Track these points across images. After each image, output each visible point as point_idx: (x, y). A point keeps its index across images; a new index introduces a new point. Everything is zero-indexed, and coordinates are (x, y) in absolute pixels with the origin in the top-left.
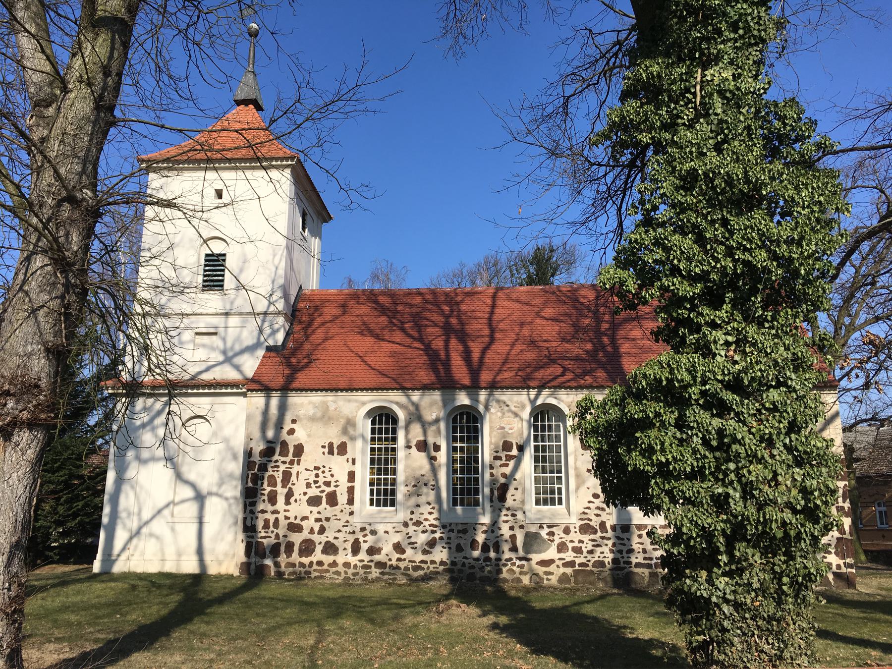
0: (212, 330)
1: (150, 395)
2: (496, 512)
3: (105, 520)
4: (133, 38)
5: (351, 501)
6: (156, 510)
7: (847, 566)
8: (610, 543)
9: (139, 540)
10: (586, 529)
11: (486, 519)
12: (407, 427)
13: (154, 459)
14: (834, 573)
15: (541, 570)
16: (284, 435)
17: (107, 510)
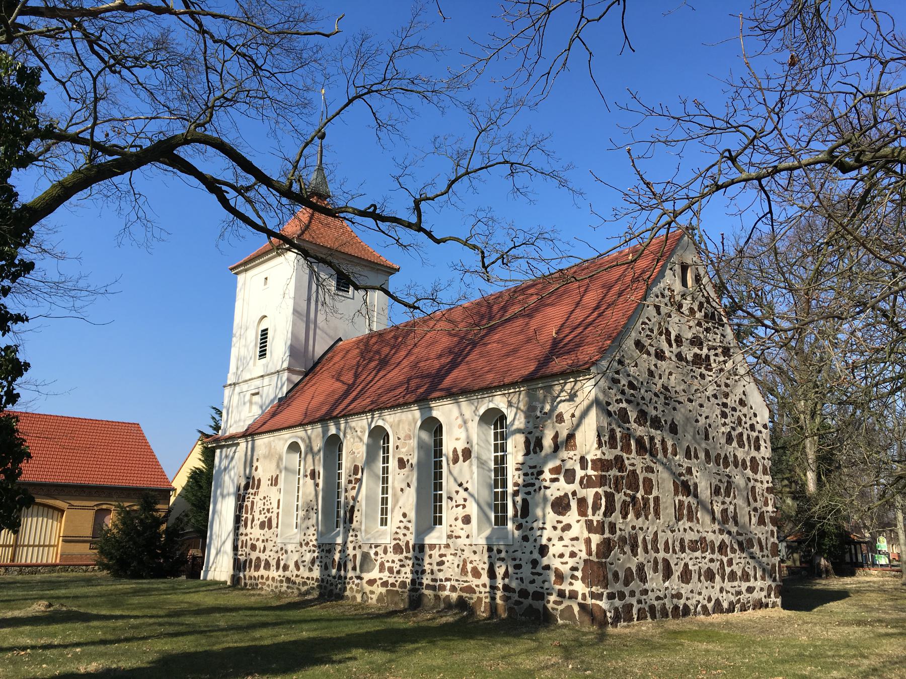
1: (228, 446)
2: (347, 531)
5: (277, 527)
7: (593, 596)
8: (410, 563)
10: (397, 549)
11: (339, 540)
14: (580, 604)
15: (368, 588)
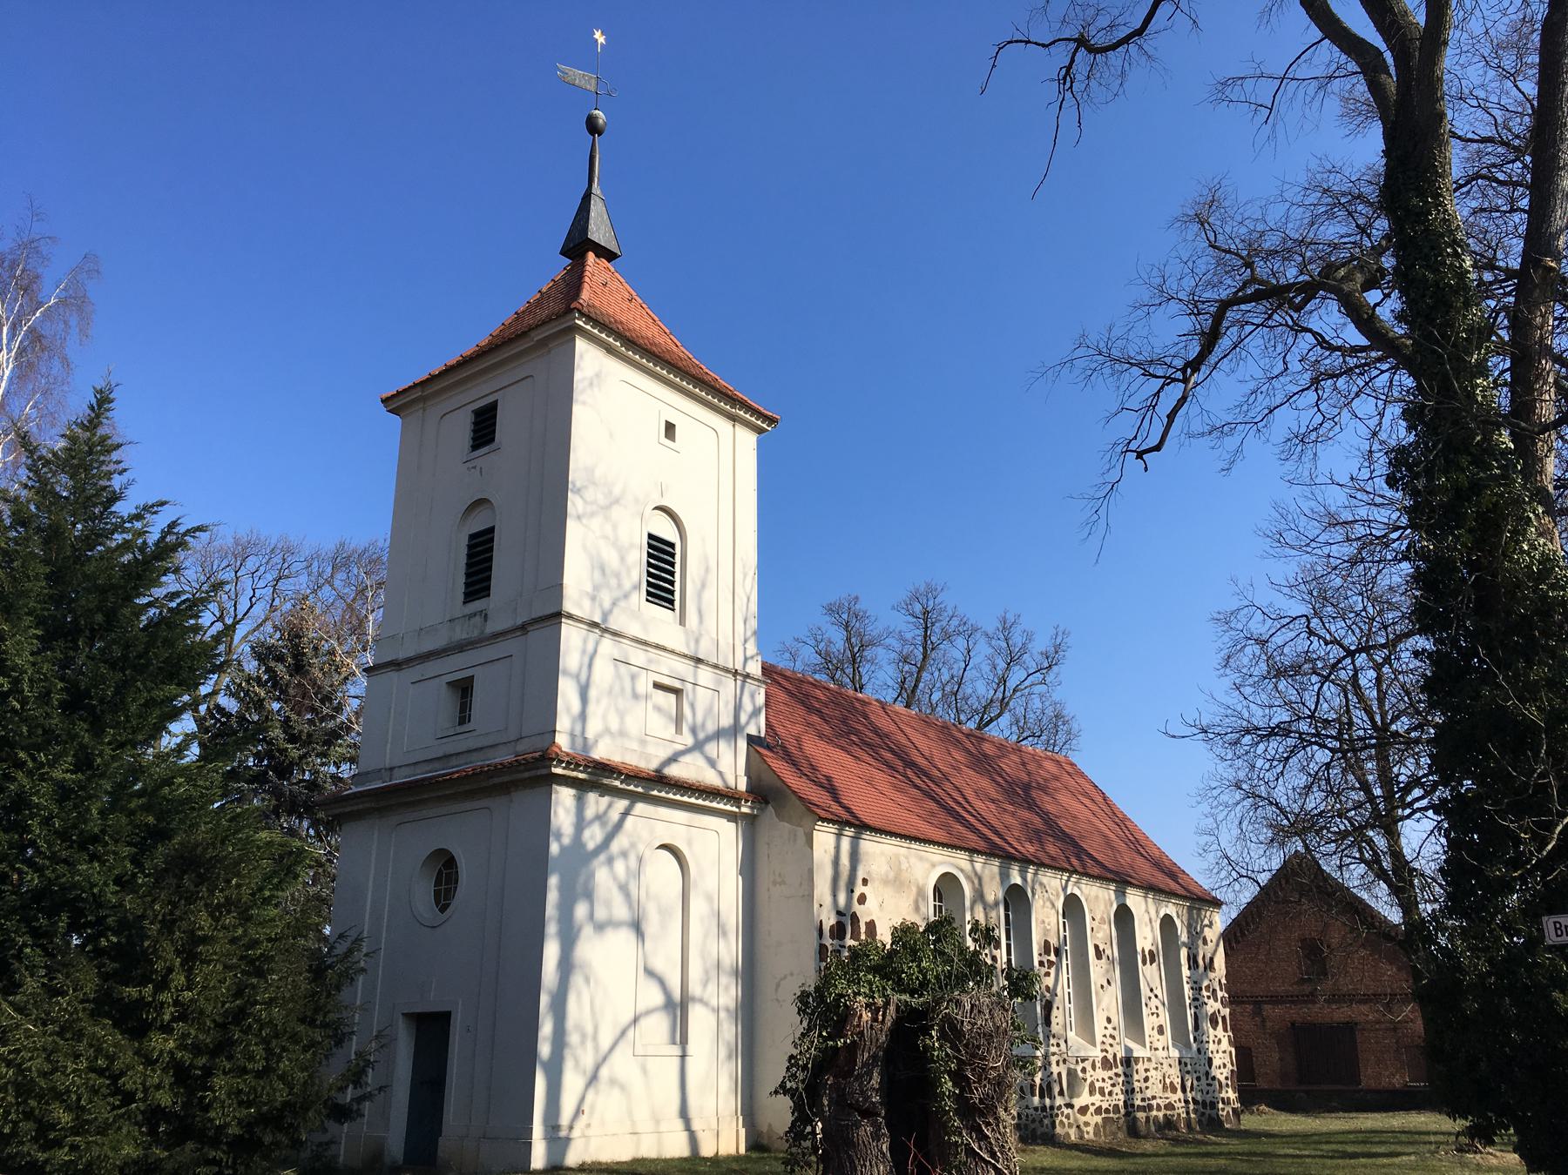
0: (677, 684)
3: (544, 1050)
4: (1301, 279)
6: (618, 1032)
9: (597, 1093)
12: (972, 909)
13: (616, 925)
16: (857, 908)
17: (546, 1028)
